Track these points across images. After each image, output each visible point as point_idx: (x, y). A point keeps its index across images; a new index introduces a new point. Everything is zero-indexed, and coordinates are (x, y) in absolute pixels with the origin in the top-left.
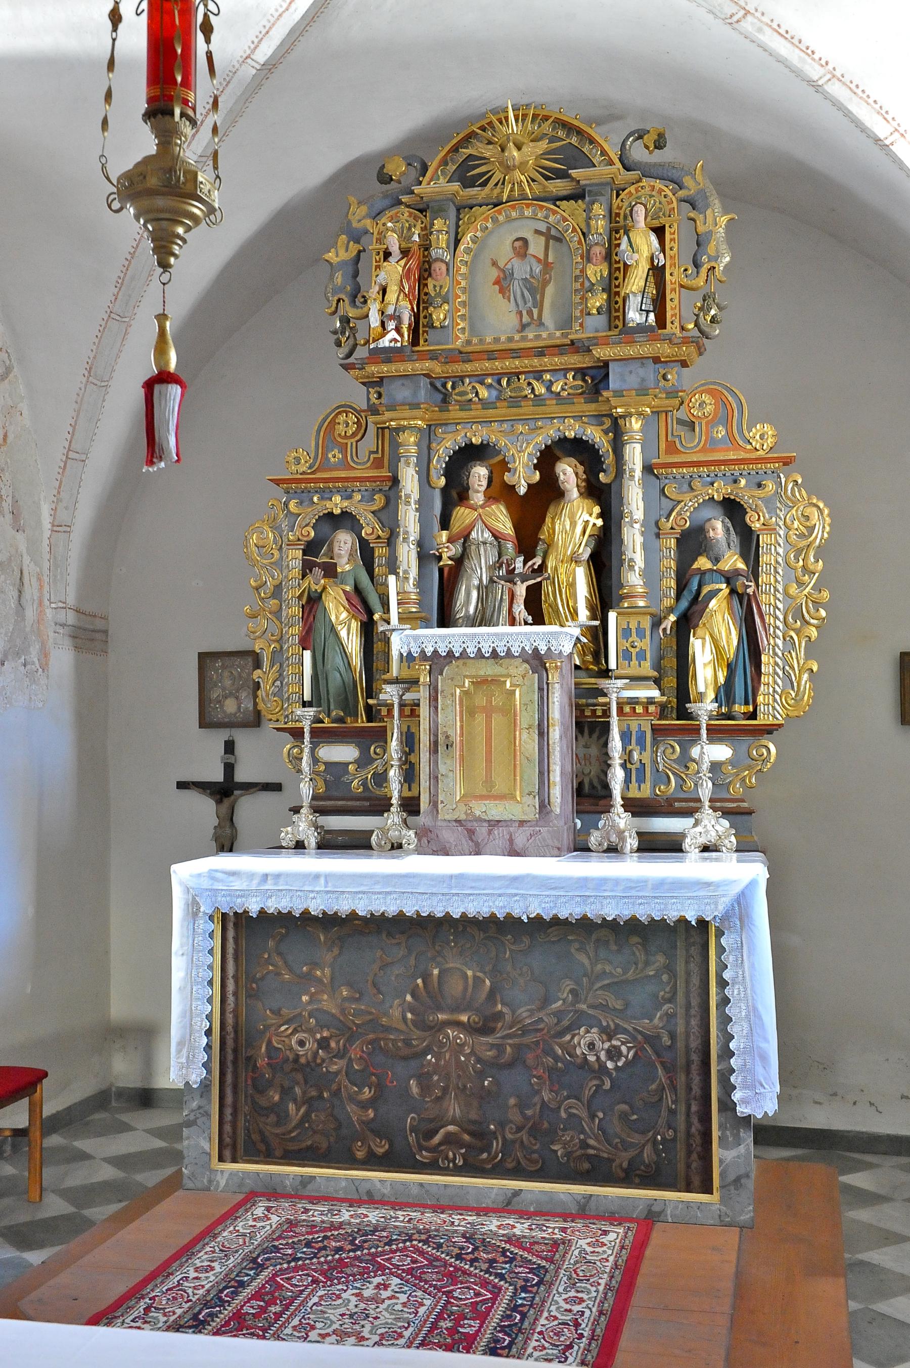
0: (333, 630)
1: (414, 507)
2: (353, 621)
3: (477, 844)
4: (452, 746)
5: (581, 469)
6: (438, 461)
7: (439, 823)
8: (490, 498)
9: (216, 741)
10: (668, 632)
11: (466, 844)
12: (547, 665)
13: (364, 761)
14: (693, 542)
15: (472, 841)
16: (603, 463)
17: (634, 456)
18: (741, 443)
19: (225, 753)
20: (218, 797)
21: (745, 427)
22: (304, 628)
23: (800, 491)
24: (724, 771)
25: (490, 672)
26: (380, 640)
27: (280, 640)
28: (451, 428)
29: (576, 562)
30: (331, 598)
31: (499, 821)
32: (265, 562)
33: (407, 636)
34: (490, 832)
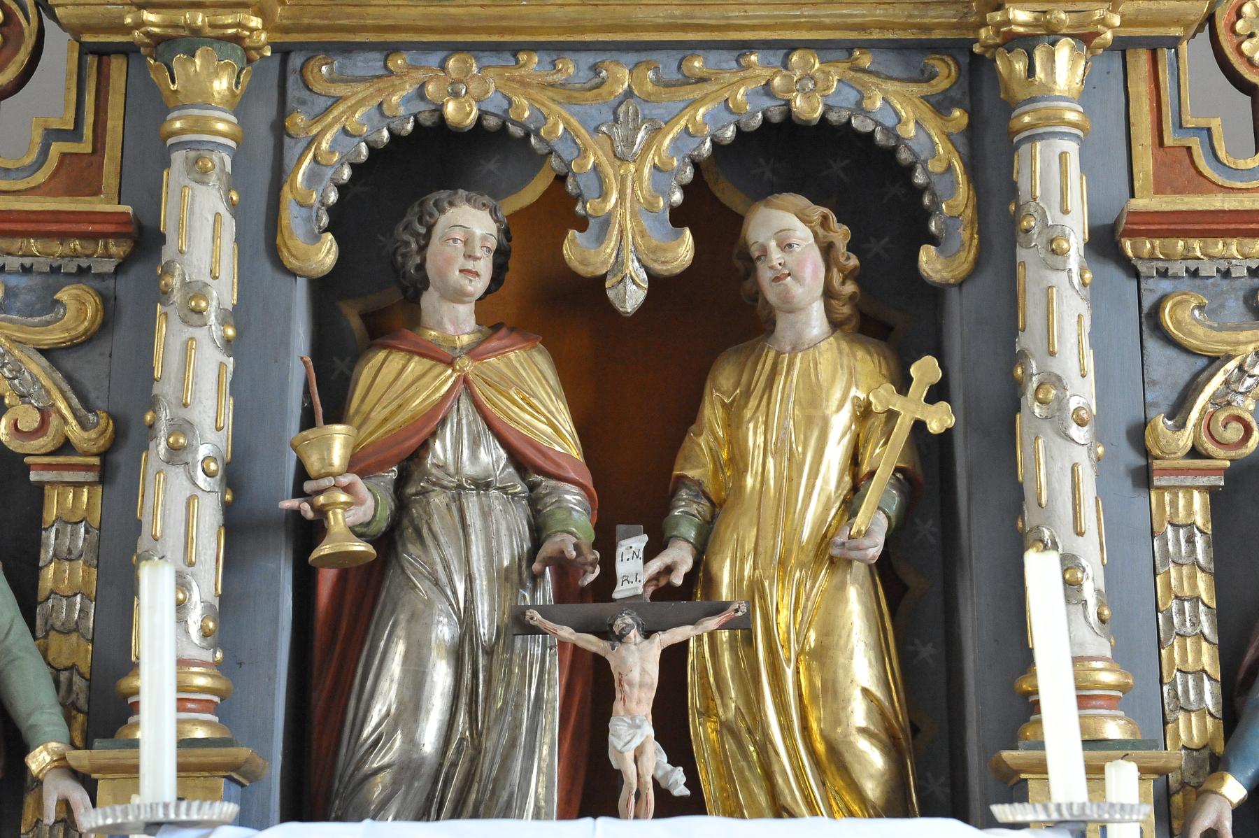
5: (840, 234)
6: (313, 178)
8: (496, 320)
16: (926, 215)
17: (1061, 188)
29: (833, 561)
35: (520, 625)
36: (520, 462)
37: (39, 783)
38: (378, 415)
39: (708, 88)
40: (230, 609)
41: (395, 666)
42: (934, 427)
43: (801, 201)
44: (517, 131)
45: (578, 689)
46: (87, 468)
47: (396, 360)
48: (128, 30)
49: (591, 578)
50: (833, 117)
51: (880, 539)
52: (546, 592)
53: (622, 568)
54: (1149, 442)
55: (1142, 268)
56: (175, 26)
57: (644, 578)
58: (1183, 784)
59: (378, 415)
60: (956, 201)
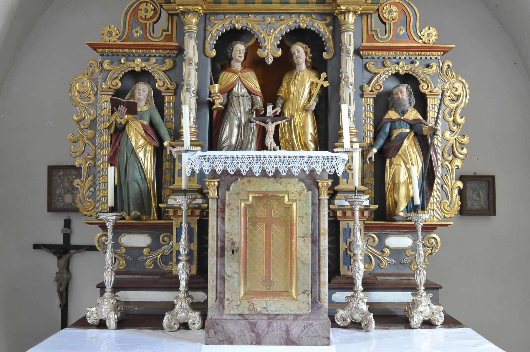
0: (133, 152)
1: (194, 67)
2: (149, 146)
3: (258, 335)
4: (237, 251)
5: (309, 50)
6: (211, 39)
7: (225, 317)
9: (58, 221)
10: (373, 160)
11: (249, 336)
12: (320, 184)
13: (154, 246)
14: (385, 102)
15: (254, 332)
16: (324, 46)
17: (350, 41)
18: (415, 38)
19: (64, 227)
20: (59, 255)
21: (418, 28)
22: (111, 151)
23: (451, 72)
24: (408, 255)
25: (271, 189)
26: (168, 160)
27: (94, 159)
28: (221, 17)
30: (132, 129)
31: (277, 315)
32: (84, 103)
33: (199, 157)
34: (269, 325)
35: (250, 121)
36: (250, 92)
37: (166, 148)
38: (224, 83)
39: (285, 22)
40: (198, 119)
41: (227, 129)
42: (325, 86)
43: (302, 44)
44: (249, 30)
45: (260, 134)
46: (172, 92)
47: (227, 73)
48: (177, 10)
49: (262, 113)
50: (308, 27)
51: (315, 106)
52: (254, 116)
53: (268, 111)
54: (363, 89)
55: (364, 57)
56: (186, 9)
57: (272, 113)
58: (366, 150)
59: (224, 83)
60: (330, 44)
